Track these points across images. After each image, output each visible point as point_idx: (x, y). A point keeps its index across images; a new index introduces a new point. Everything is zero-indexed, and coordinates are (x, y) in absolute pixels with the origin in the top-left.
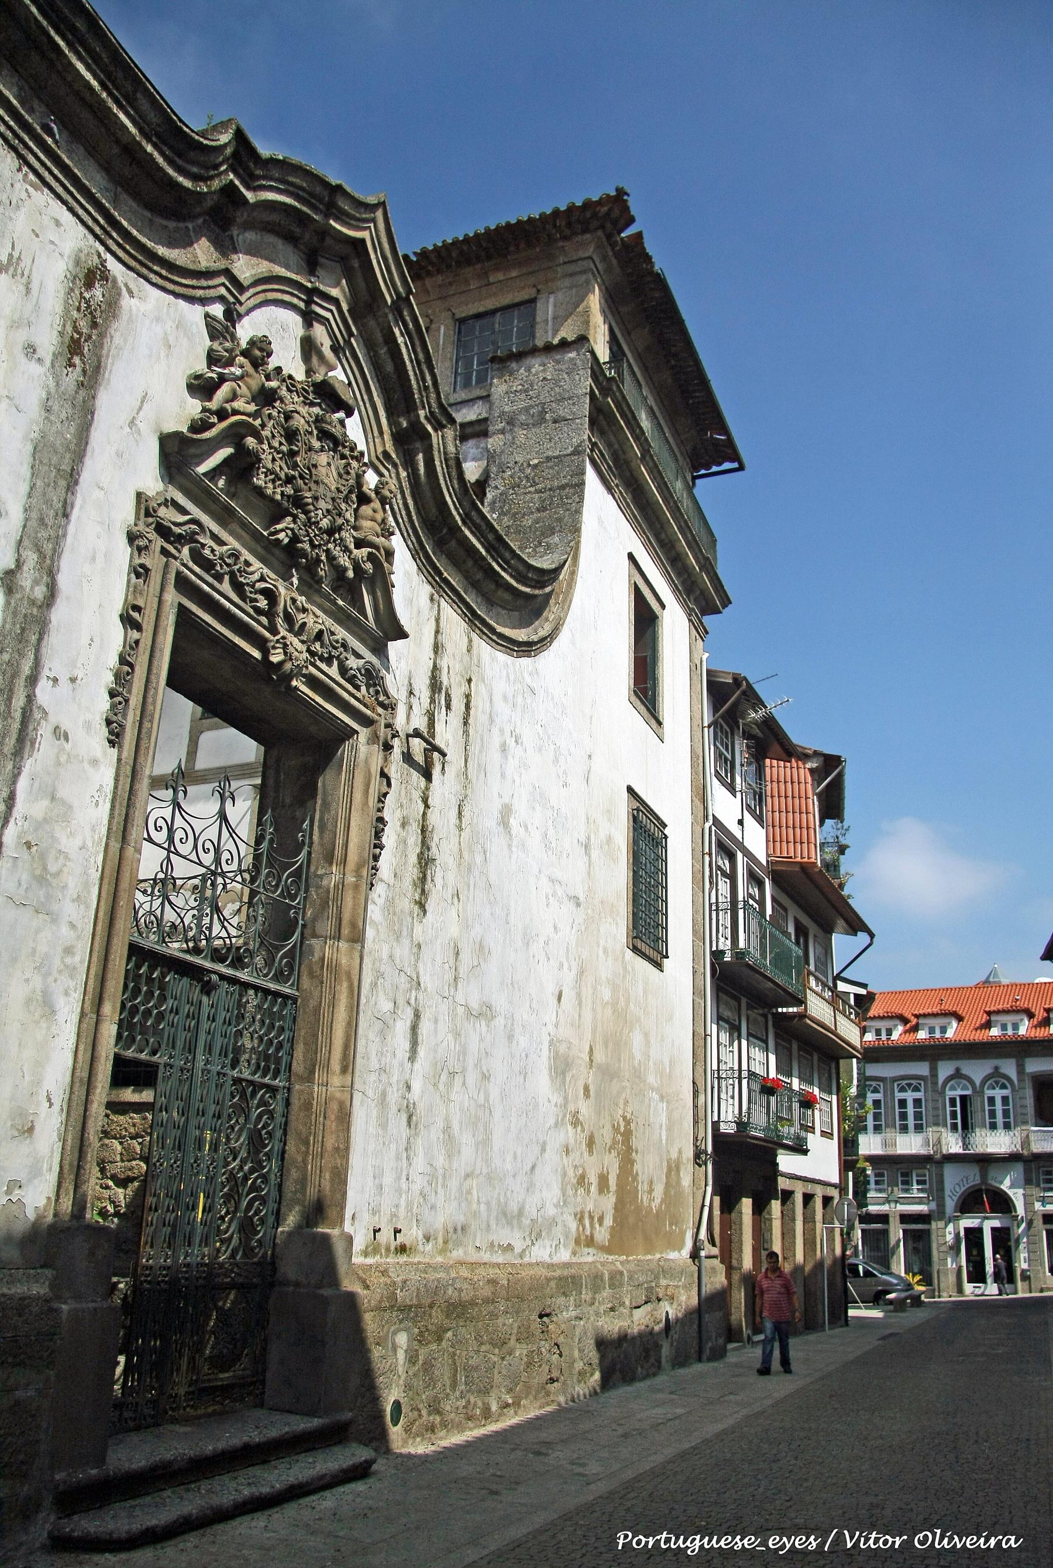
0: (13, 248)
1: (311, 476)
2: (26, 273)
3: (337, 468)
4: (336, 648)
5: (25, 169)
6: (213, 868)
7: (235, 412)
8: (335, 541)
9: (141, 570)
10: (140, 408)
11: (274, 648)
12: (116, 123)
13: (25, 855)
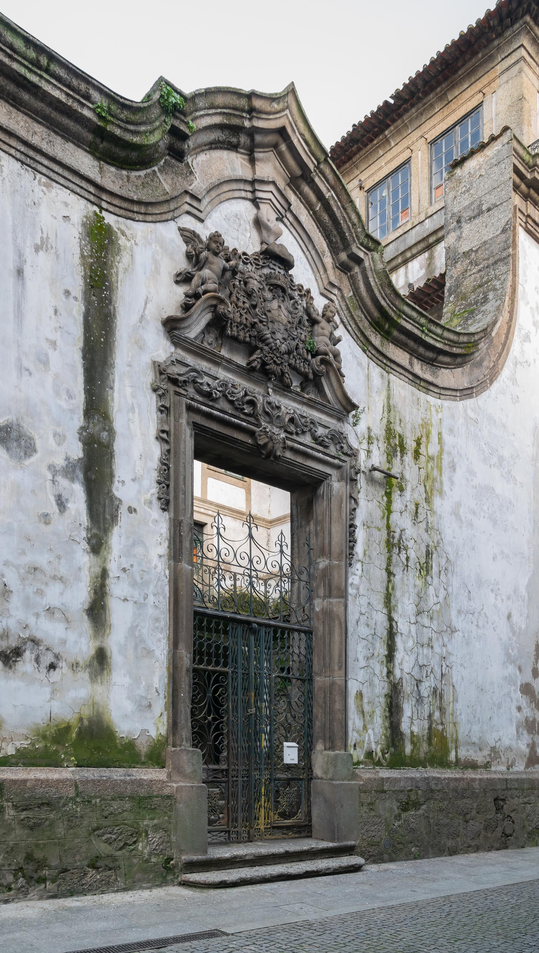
0: (42, 233)
1: (267, 318)
2: (54, 246)
3: (286, 309)
4: (306, 426)
5: (39, 176)
6: (249, 567)
7: (205, 292)
8: (294, 357)
9: (163, 409)
10: (145, 308)
11: (260, 435)
12: (83, 119)
13: (123, 575)
